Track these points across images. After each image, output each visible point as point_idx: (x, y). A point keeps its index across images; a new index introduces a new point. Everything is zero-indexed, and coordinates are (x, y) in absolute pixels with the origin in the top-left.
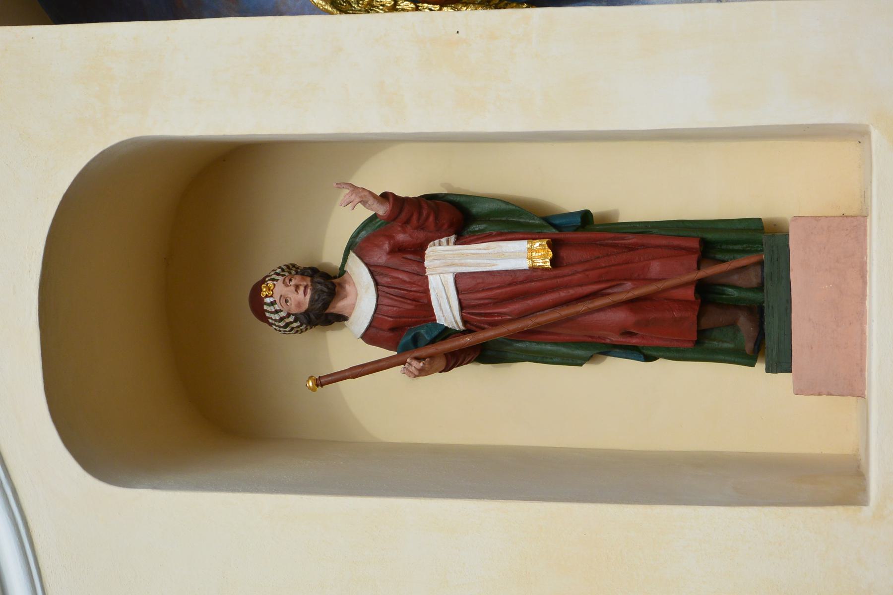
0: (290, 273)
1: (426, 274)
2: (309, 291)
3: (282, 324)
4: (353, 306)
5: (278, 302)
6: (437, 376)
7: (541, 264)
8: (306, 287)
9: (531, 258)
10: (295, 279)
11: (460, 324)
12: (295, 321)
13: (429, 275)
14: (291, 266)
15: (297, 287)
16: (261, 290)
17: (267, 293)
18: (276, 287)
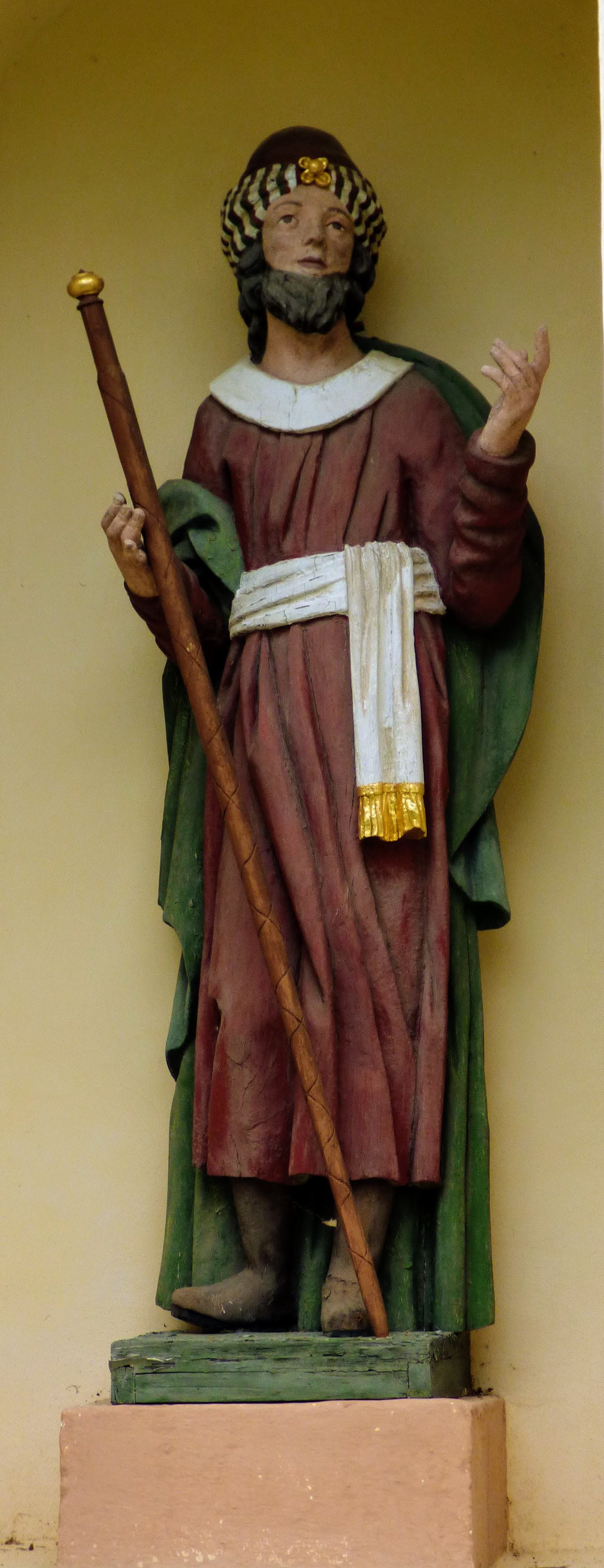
0: (358, 223)
1: (346, 546)
2: (308, 271)
3: (238, 210)
4: (276, 374)
5: (286, 197)
6: (118, 578)
7: (367, 816)
8: (320, 263)
9: (383, 791)
10: (341, 237)
11: (250, 623)
12: (247, 240)
13: (345, 556)
14: (376, 223)
15: (320, 243)
16: (314, 157)
17: (307, 171)
18: (324, 192)
